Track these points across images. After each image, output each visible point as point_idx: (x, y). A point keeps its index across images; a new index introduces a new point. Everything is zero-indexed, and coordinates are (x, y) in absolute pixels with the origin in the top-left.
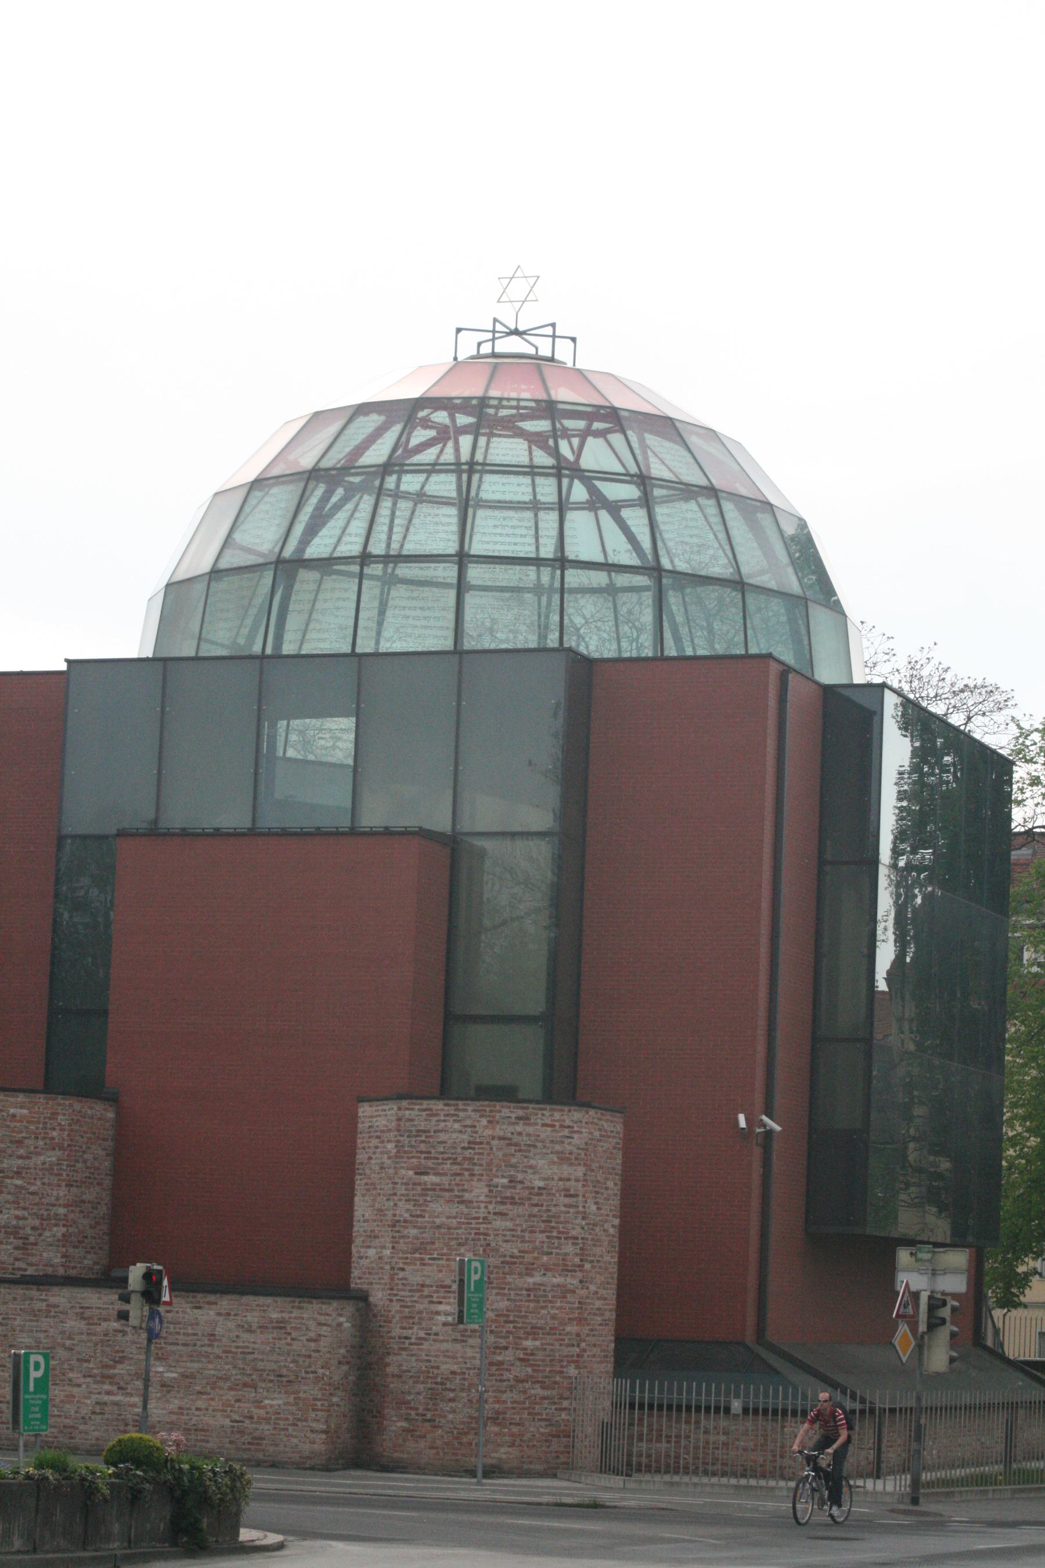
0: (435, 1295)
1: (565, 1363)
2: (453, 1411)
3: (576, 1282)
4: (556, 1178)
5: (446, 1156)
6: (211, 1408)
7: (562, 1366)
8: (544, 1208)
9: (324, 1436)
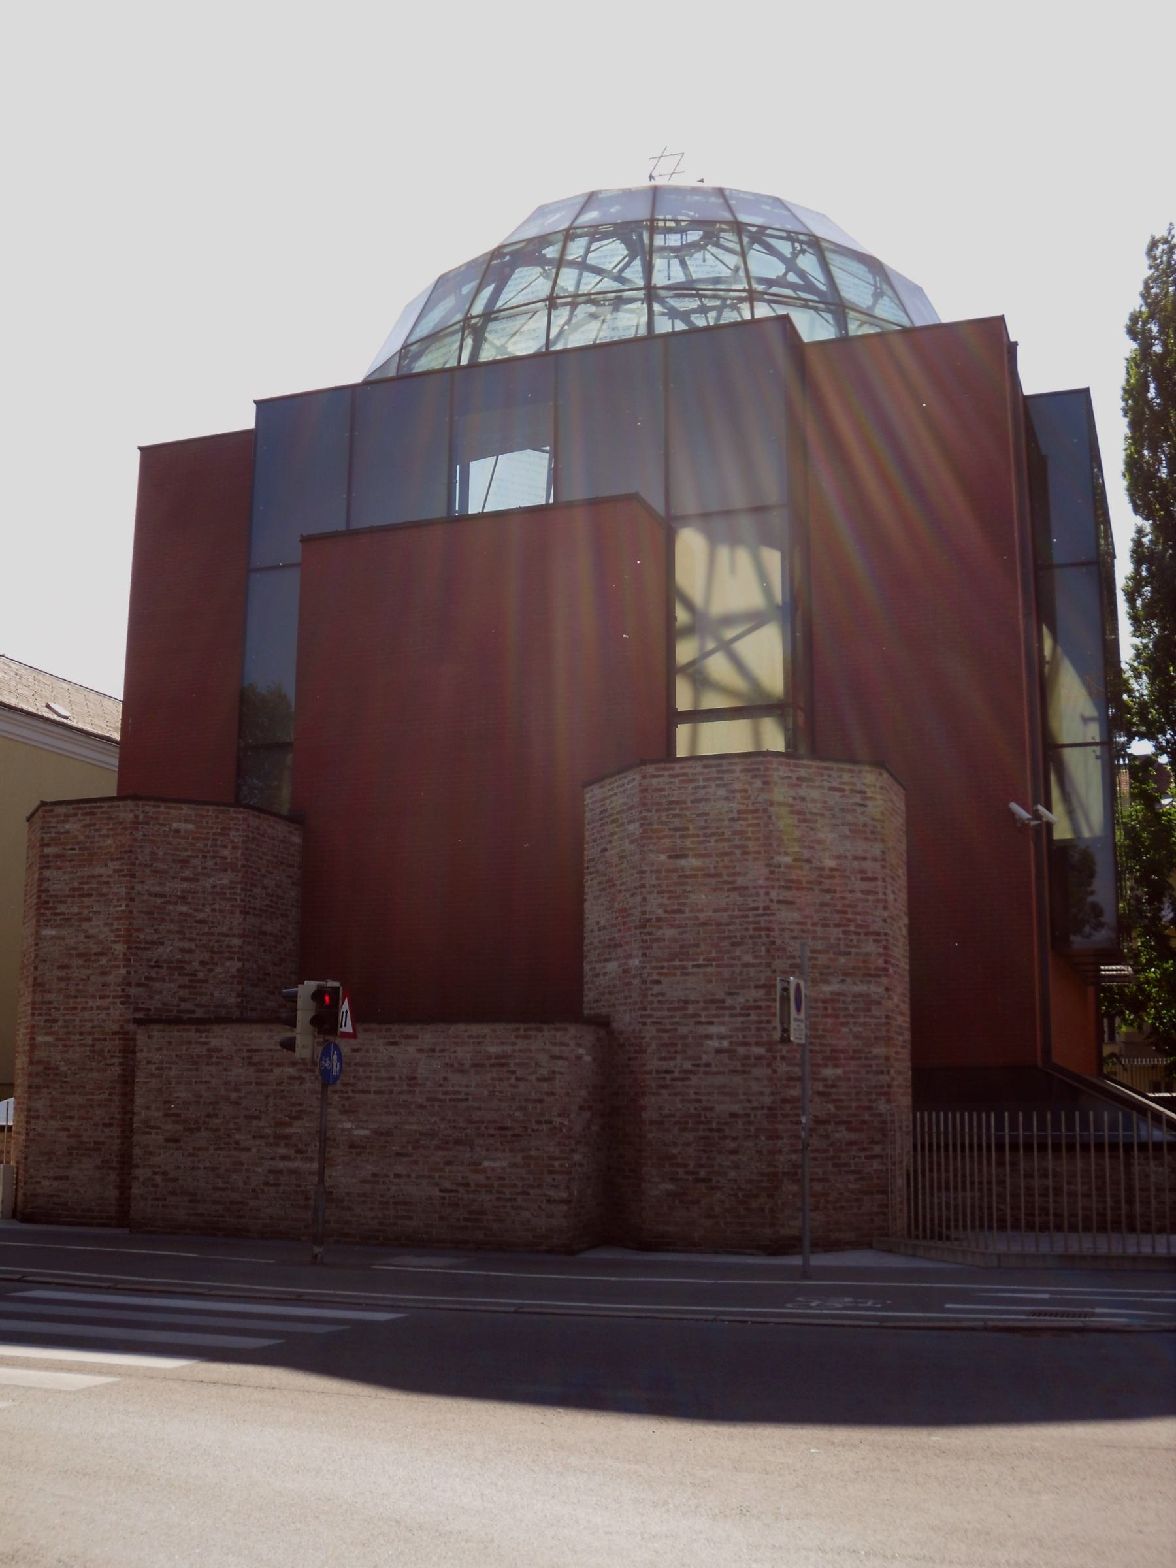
0: (703, 1014)
2: (736, 1166)
3: (881, 990)
5: (709, 831)
6: (414, 1175)
7: (870, 1101)
8: (838, 895)
9: (565, 1208)
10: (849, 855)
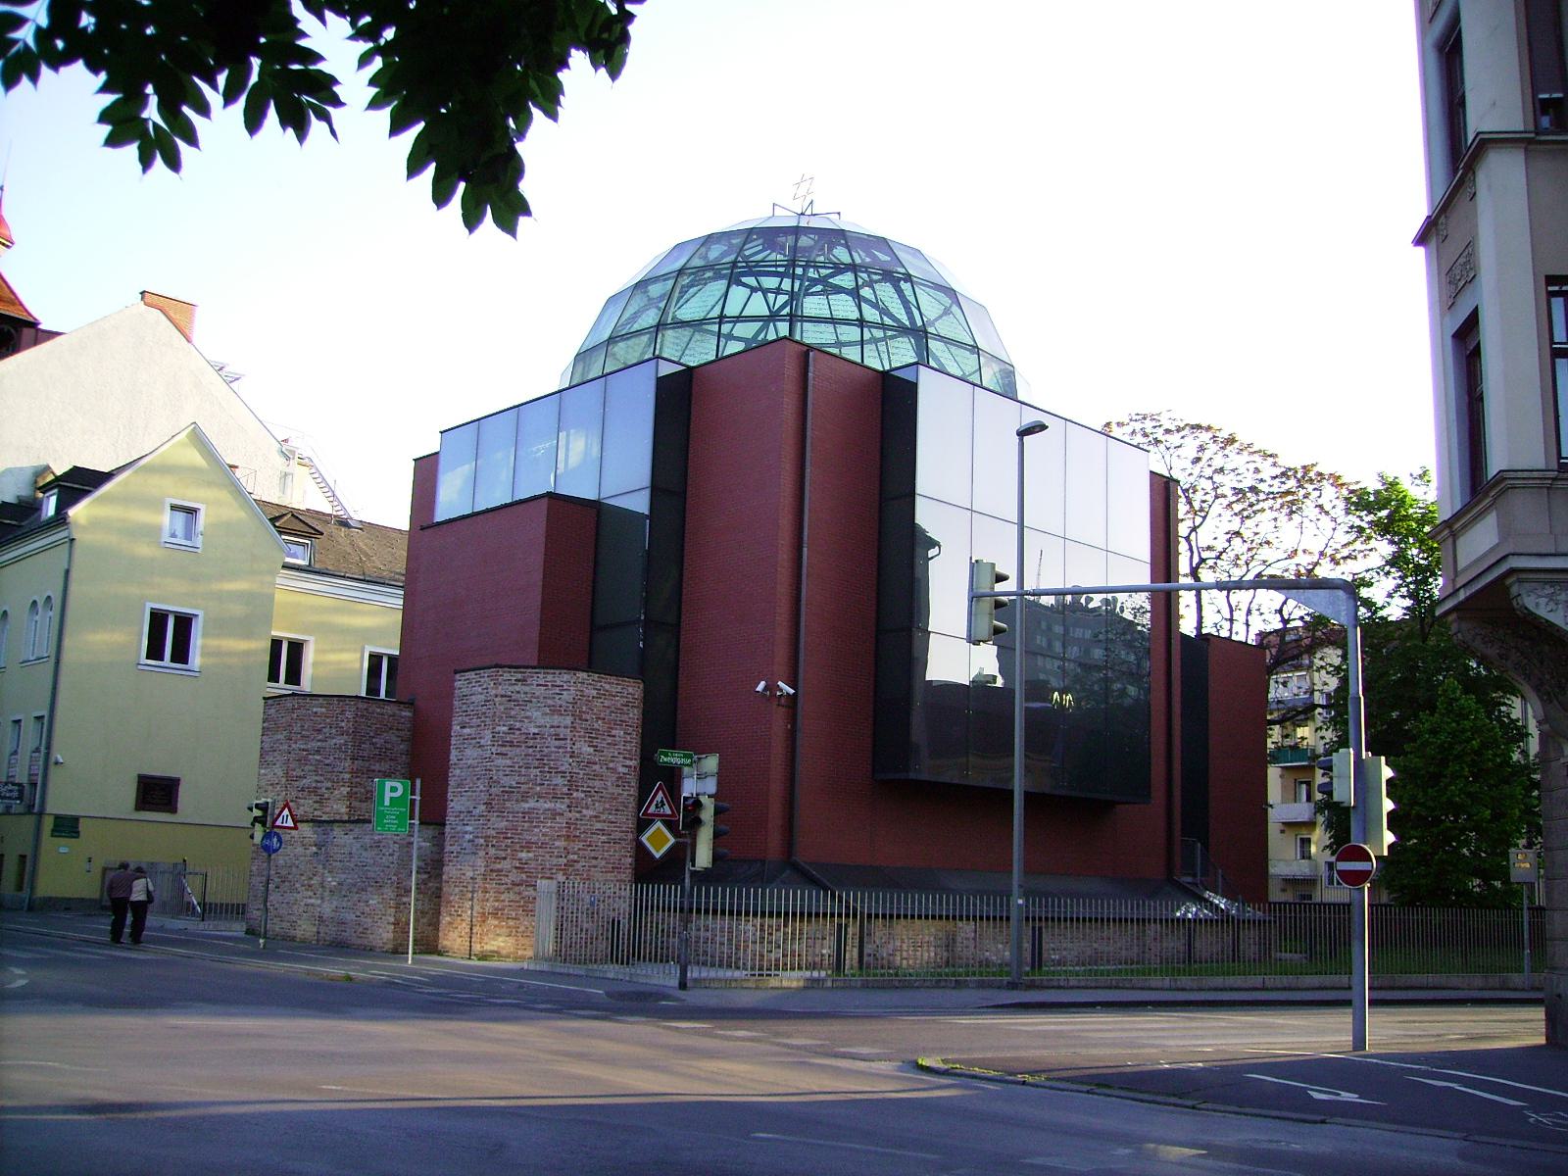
1: (554, 871)
4: (548, 725)
8: (538, 749)
10: (548, 725)
